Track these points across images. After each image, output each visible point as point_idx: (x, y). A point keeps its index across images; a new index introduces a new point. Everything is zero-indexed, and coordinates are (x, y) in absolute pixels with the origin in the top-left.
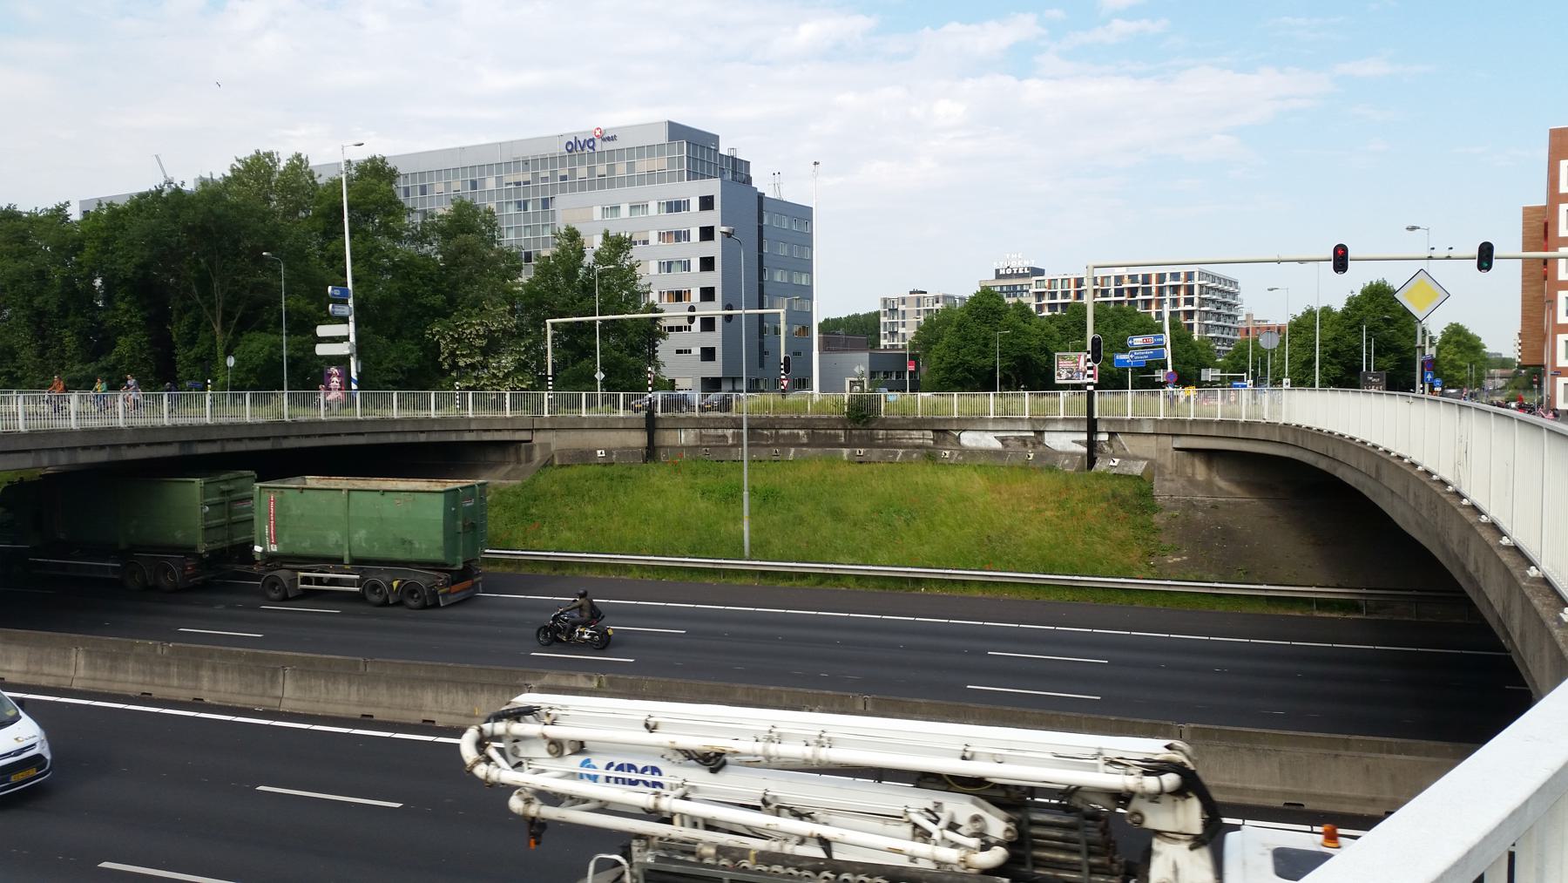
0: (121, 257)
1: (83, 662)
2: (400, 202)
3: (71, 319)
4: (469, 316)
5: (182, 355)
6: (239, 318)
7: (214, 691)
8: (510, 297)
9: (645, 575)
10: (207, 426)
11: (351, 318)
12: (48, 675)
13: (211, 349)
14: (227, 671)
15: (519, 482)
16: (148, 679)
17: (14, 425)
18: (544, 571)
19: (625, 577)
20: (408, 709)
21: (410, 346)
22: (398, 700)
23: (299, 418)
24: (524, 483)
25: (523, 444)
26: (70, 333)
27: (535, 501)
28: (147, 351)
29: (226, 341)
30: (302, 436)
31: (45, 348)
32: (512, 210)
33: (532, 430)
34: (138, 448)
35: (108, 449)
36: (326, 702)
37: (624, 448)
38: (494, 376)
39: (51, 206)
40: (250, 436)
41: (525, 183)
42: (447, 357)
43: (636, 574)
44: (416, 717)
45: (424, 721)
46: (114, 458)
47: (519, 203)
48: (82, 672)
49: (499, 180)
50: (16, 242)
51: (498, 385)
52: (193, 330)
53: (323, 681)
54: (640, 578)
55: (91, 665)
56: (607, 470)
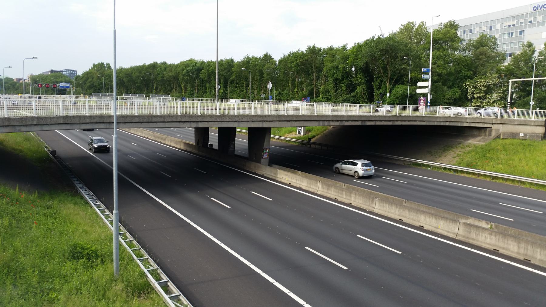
0: (360, 60)
1: (321, 186)
2: (458, 37)
3: (344, 81)
4: (481, 78)
5: (376, 92)
6: (395, 80)
7: (355, 202)
8: (499, 71)
9: (532, 187)
10: (371, 116)
11: (430, 80)
12: (312, 188)
13: (385, 90)
14: (359, 196)
15: (484, 143)
16: (337, 194)
17: (163, 112)
18: (488, 179)
19: (522, 186)
20: (415, 220)
21: (457, 90)
22: (412, 217)
23: (402, 115)
24: (486, 144)
25: (488, 129)
26: (344, 85)
27: (489, 151)
28: (366, 91)
29: (390, 88)
30: (403, 121)
31: (337, 90)
32: (506, 36)
33: (492, 123)
34: (348, 122)
35: (339, 122)
36: (388, 212)
37: (533, 133)
38: (489, 102)
39: (343, 45)
40: (384, 120)
41: (513, 25)
42: (470, 94)
43: (528, 186)
44: (417, 224)
45: (420, 226)
46: (341, 124)
47: (509, 34)
48: (320, 189)
49: (502, 25)
50: (331, 57)
51: (490, 105)
52: (380, 84)
53: (388, 205)
54: (529, 188)
55: (323, 188)
56: (523, 142)
